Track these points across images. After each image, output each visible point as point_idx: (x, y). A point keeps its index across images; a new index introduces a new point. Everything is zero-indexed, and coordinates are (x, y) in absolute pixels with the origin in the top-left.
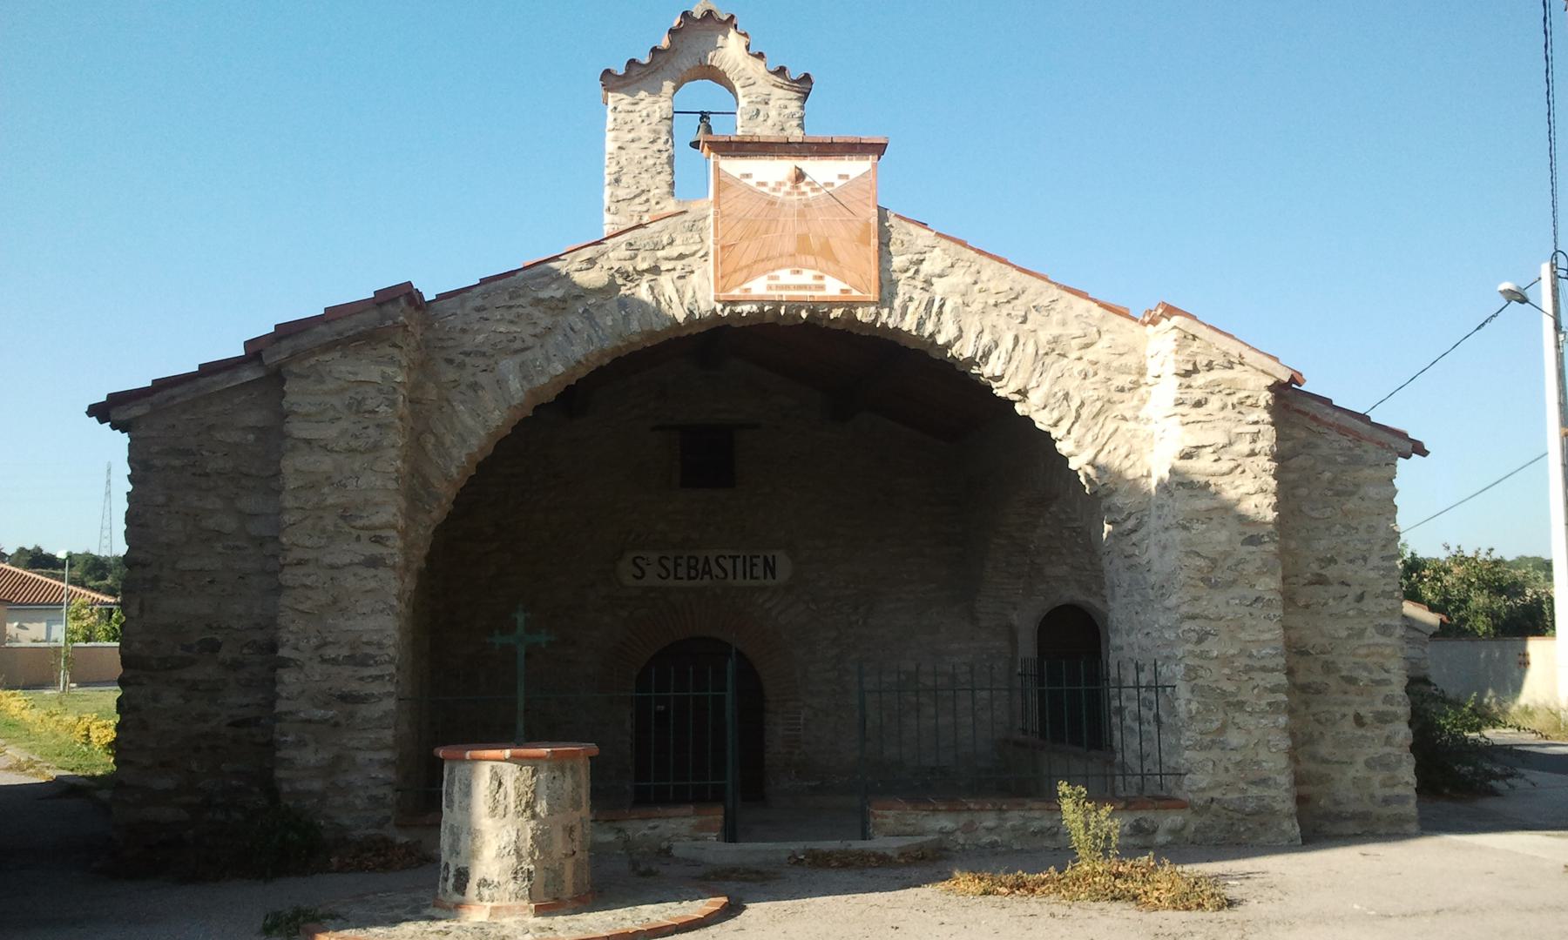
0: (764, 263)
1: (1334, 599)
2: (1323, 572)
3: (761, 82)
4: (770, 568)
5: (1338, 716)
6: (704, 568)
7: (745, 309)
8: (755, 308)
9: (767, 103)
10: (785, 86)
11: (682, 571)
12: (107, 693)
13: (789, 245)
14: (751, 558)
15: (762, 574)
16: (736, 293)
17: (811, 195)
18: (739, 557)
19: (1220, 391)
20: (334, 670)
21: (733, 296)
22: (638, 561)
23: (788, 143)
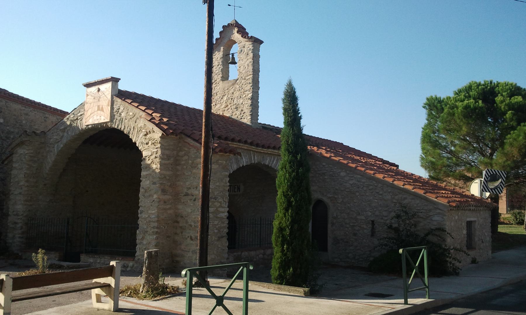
1: (189, 200)
2: (188, 192)
3: (243, 41)
4: (239, 189)
5: (187, 236)
7: (90, 126)
9: (244, 47)
10: (248, 41)
12: (518, 228)
14: (235, 186)
19: (151, 139)
23: (96, 82)
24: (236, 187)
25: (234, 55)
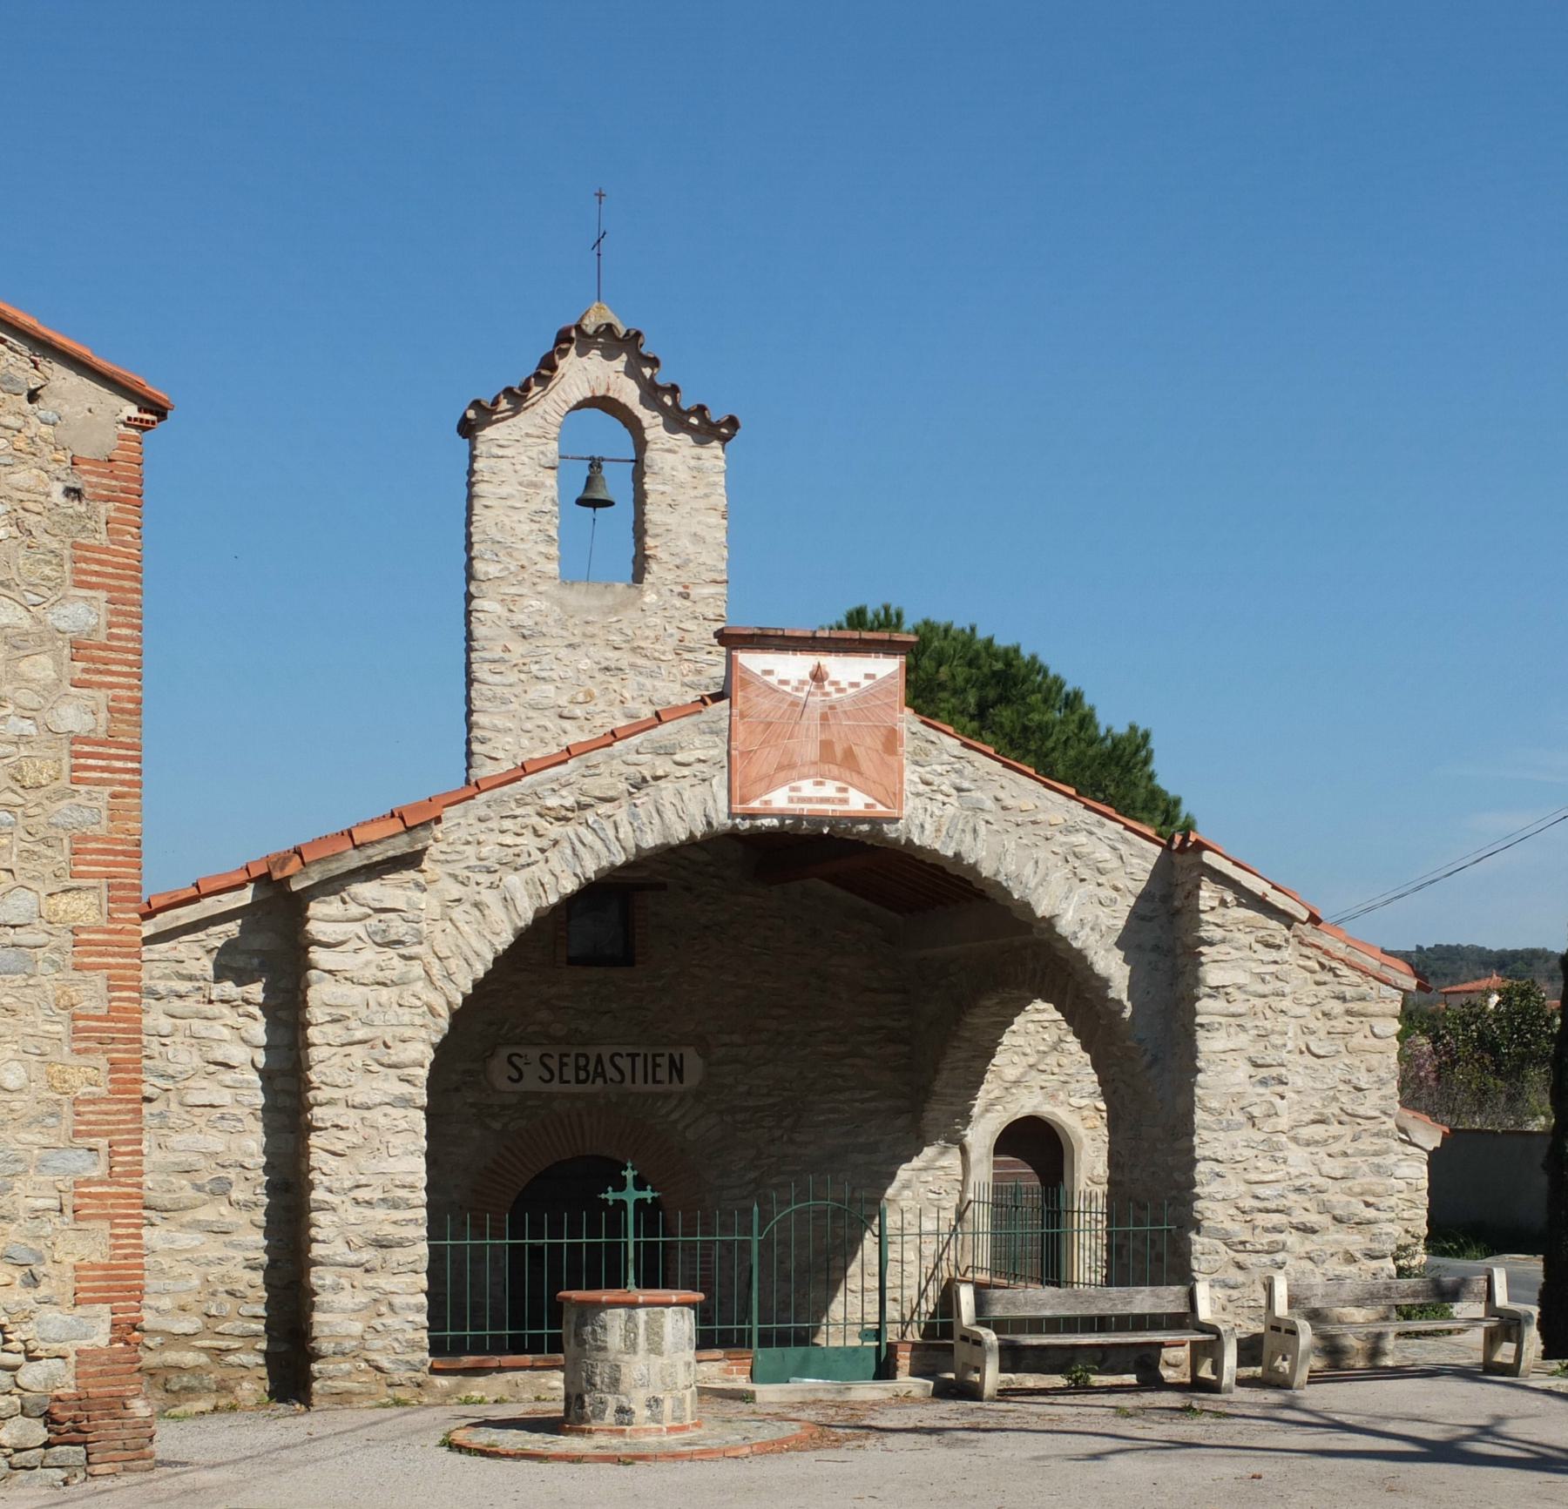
0: (787, 769)
4: (677, 1069)
6: (596, 1068)
8: (775, 822)
11: (569, 1073)
13: (812, 751)
14: (654, 1056)
15: (667, 1079)
16: (755, 804)
17: (836, 696)
18: (638, 1055)
20: (368, 1212)
21: (753, 809)
22: (515, 1059)
24: (658, 1060)
25: (600, 467)
